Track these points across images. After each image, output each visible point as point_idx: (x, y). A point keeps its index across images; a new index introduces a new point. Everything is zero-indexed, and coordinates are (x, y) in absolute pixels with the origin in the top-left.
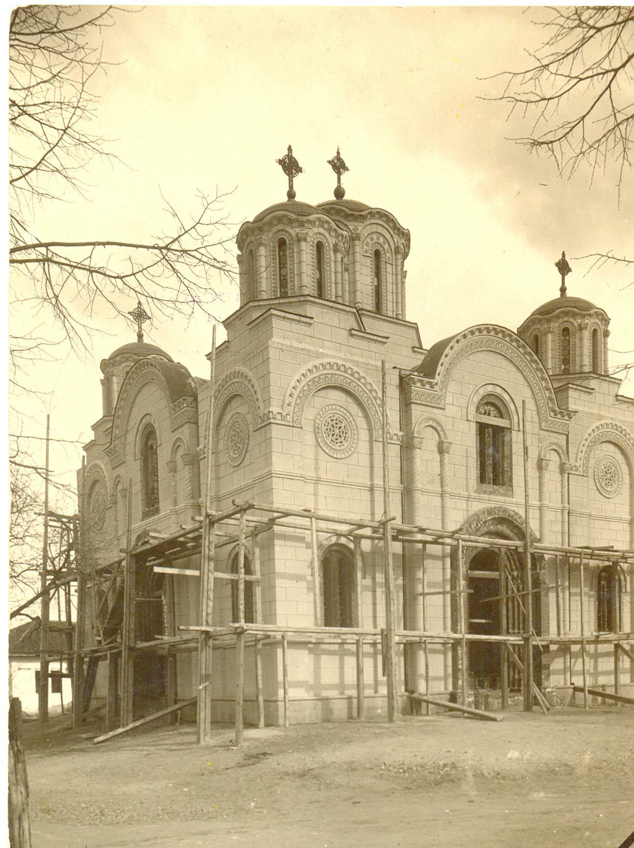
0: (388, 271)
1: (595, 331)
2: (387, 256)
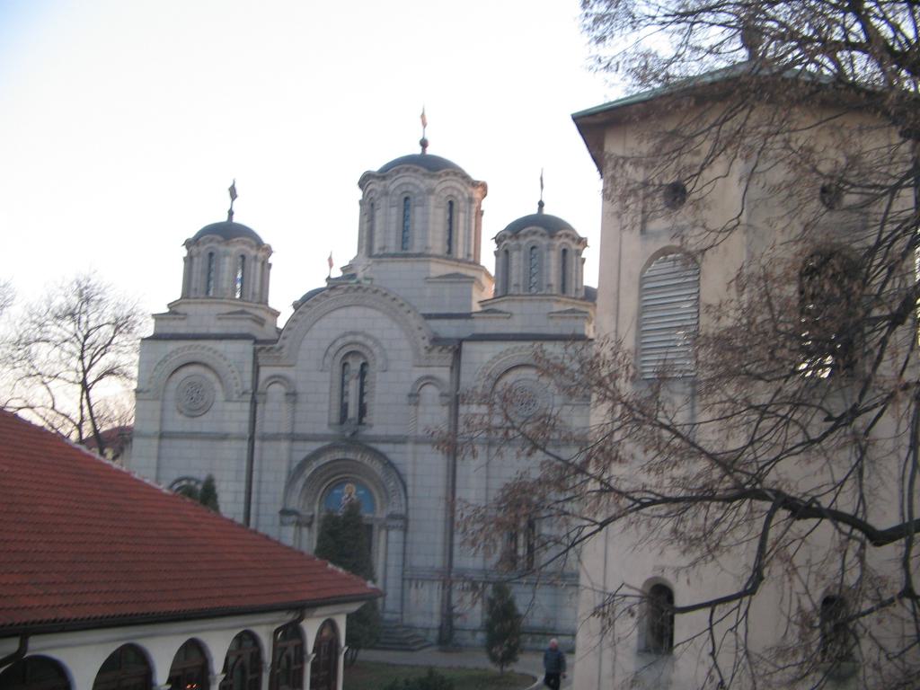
0: (461, 219)
1: (565, 251)
2: (461, 204)
